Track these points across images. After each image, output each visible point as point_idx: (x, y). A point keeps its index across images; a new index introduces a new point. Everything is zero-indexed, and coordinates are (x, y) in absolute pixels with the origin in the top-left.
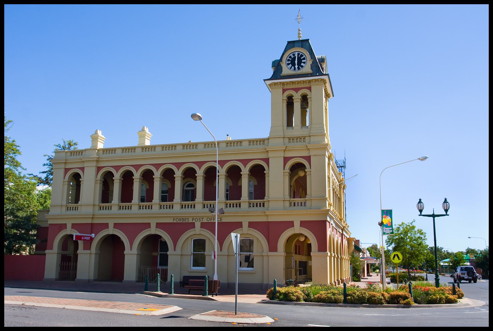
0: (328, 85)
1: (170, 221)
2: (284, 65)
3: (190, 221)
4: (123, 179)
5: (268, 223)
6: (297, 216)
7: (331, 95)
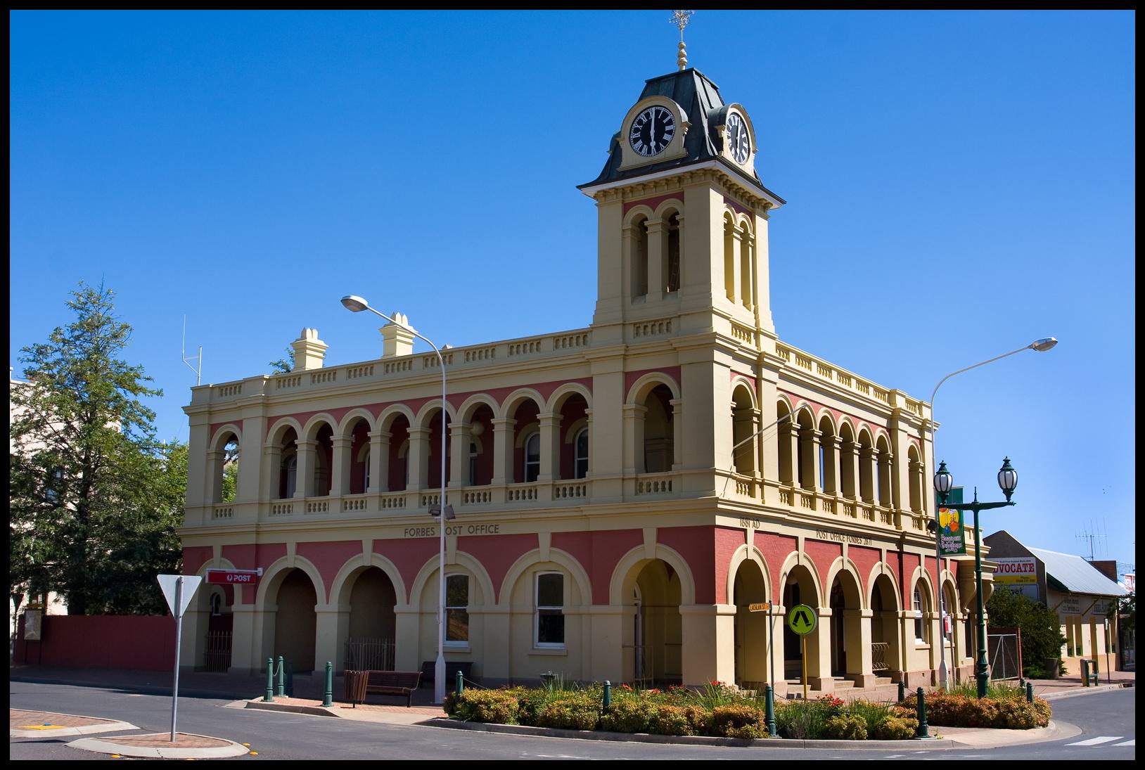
1: (399, 534)
2: (625, 145)
4: (391, 435)
5: (589, 535)
6: (653, 515)
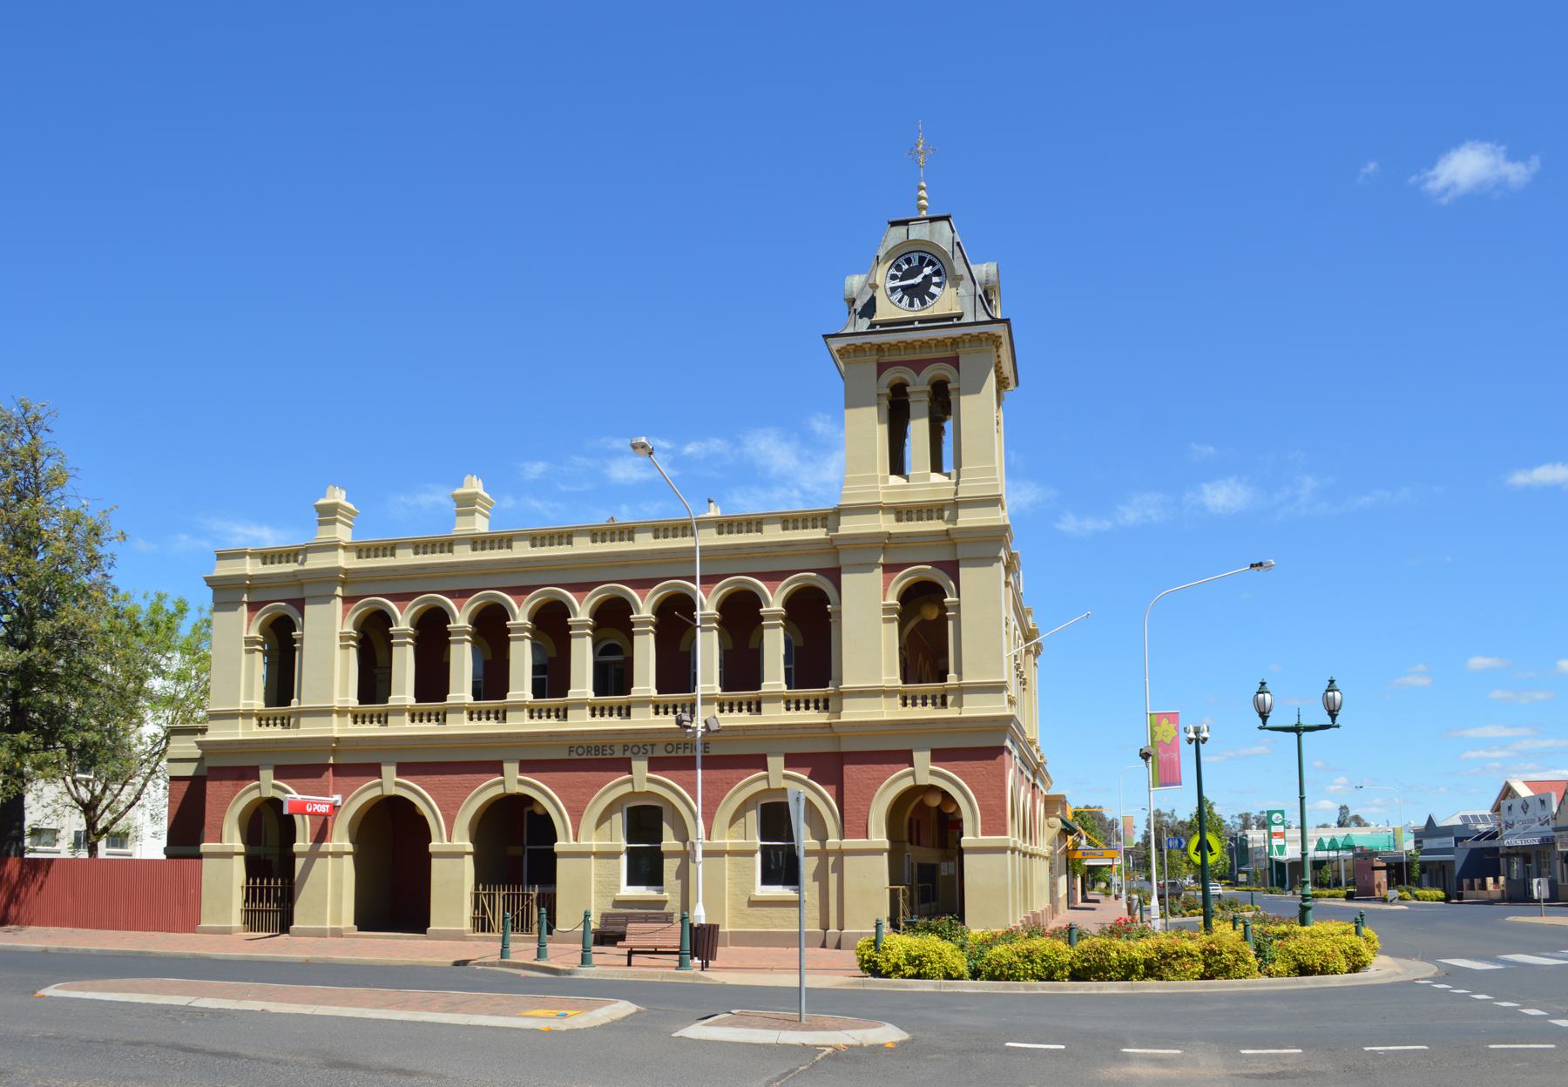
0: (1005, 351)
3: (618, 754)
7: (1012, 380)
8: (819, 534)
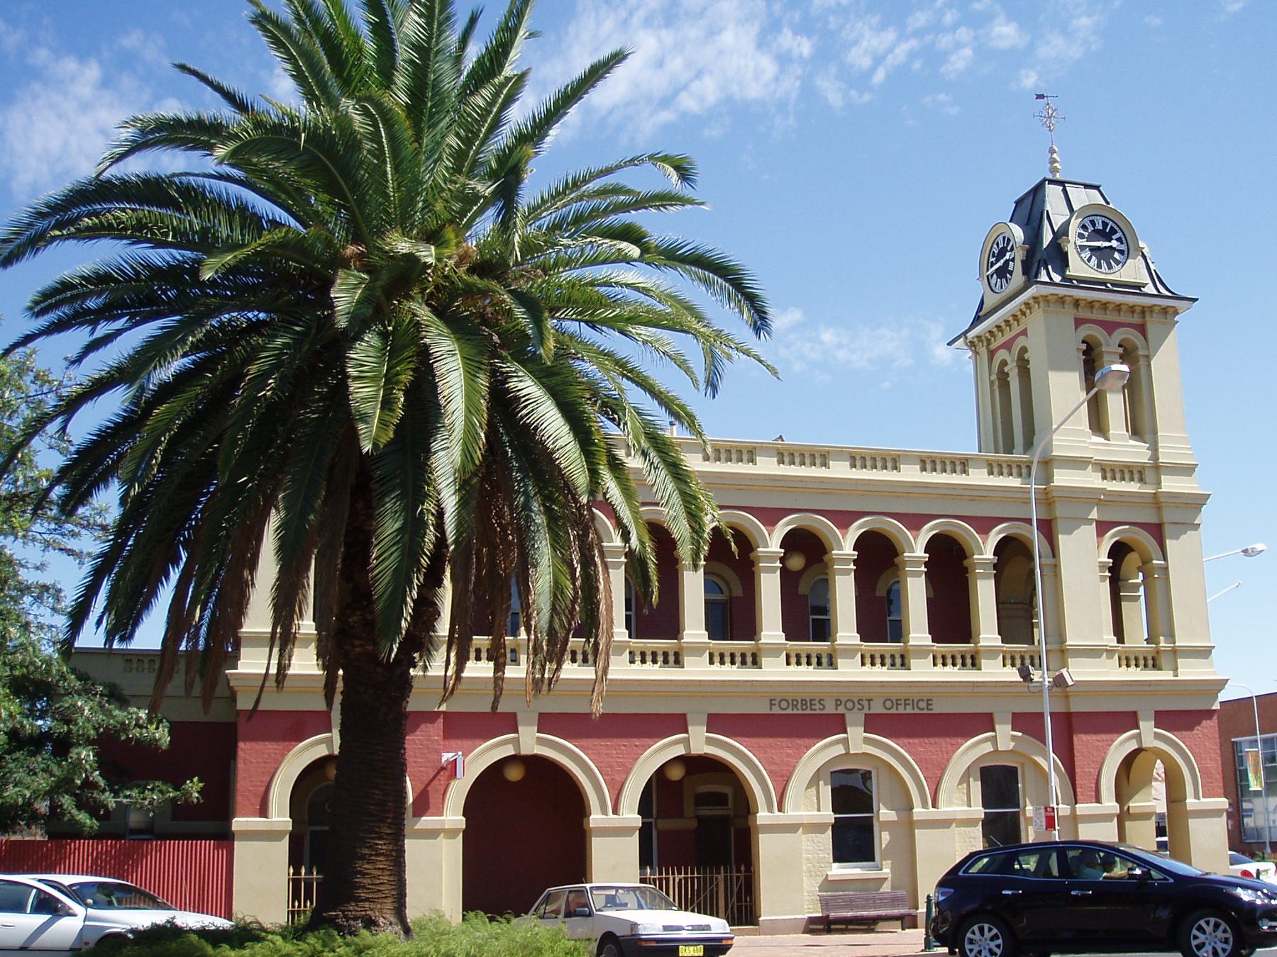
3: (830, 709)
8: (1133, 487)
